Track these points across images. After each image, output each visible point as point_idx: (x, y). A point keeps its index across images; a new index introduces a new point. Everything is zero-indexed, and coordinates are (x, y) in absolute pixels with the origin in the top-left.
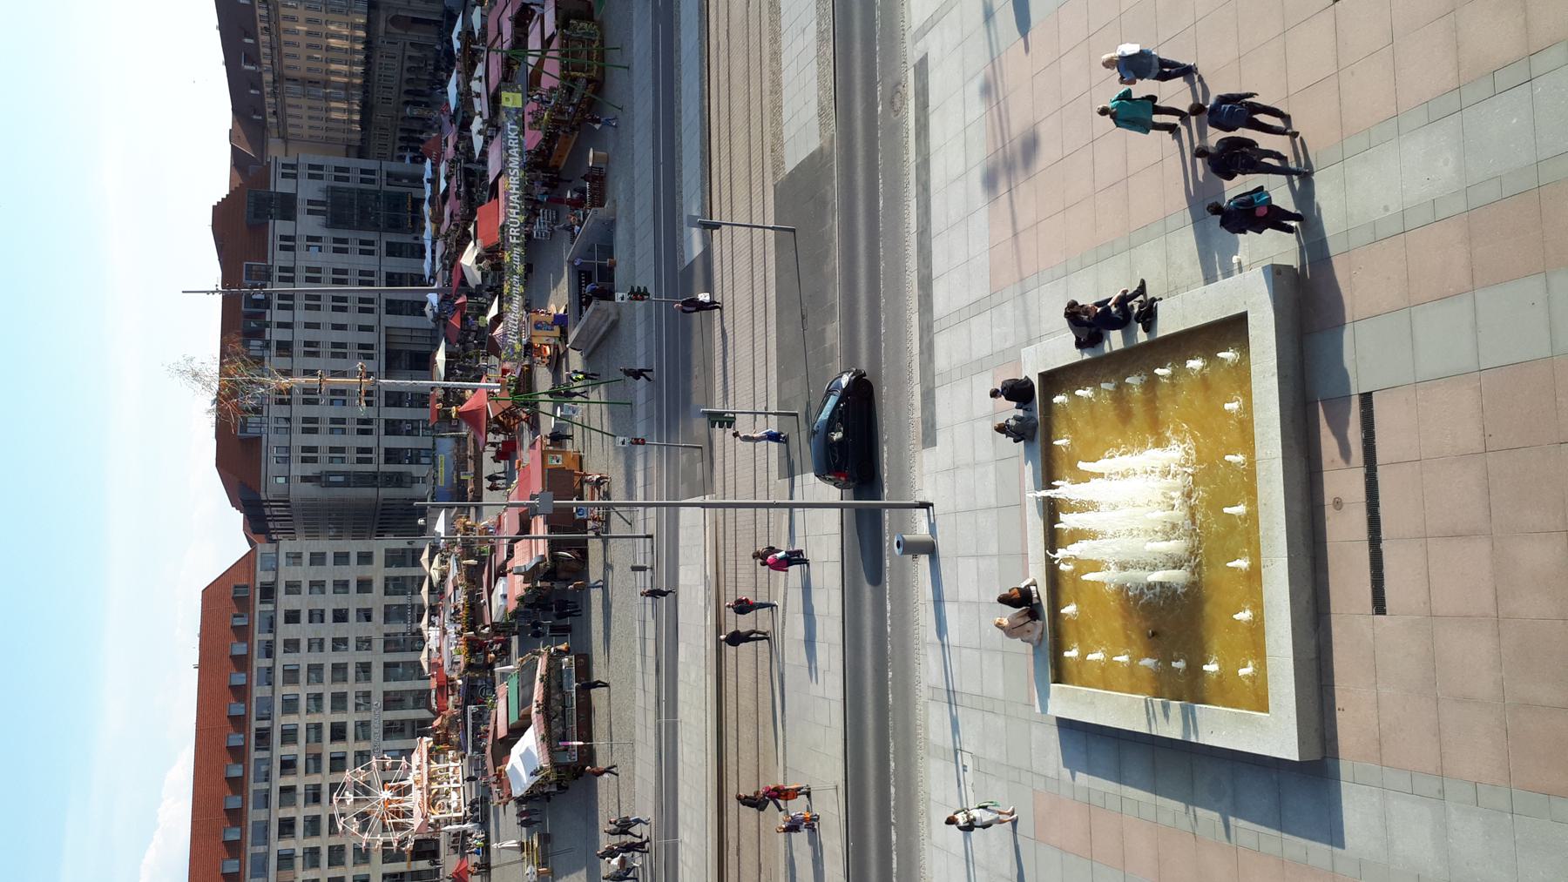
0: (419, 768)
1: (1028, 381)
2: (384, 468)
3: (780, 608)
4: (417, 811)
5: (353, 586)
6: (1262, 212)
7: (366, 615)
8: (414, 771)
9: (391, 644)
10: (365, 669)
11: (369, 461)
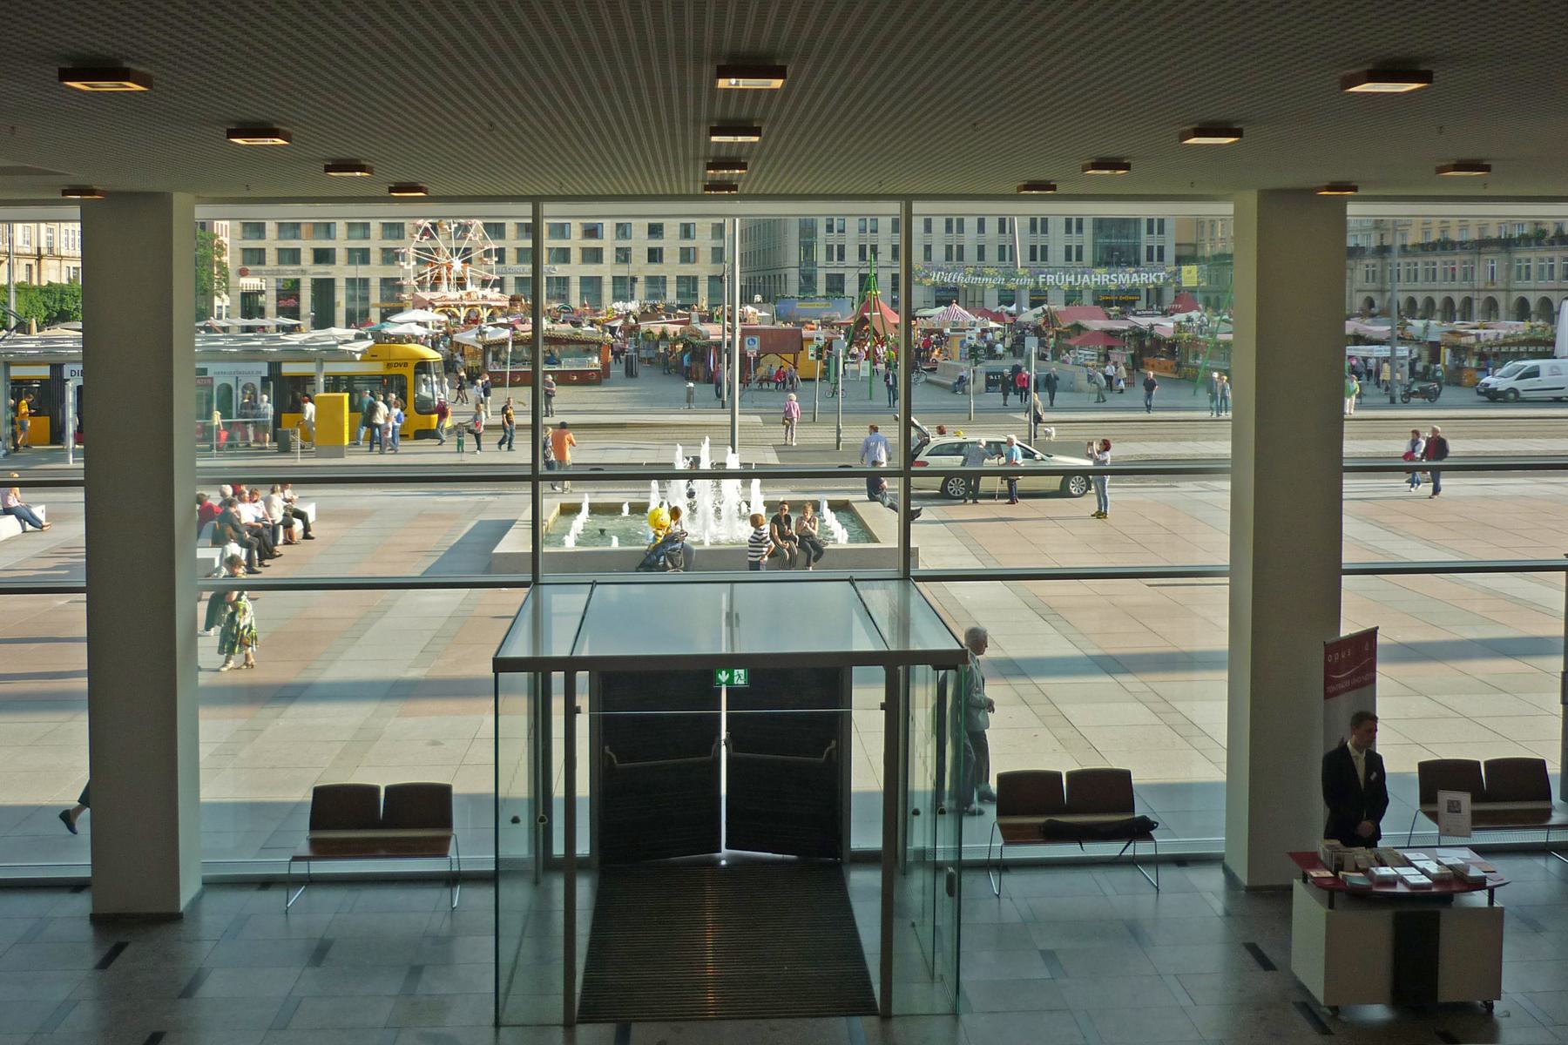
0: (484, 297)
1: (1059, 775)
2: (821, 276)
3: (440, 449)
4: (436, 295)
5: (687, 243)
6: (1264, 980)
7: (655, 255)
8: (481, 293)
9: (324, 289)
10: (594, 256)
11: (830, 257)
